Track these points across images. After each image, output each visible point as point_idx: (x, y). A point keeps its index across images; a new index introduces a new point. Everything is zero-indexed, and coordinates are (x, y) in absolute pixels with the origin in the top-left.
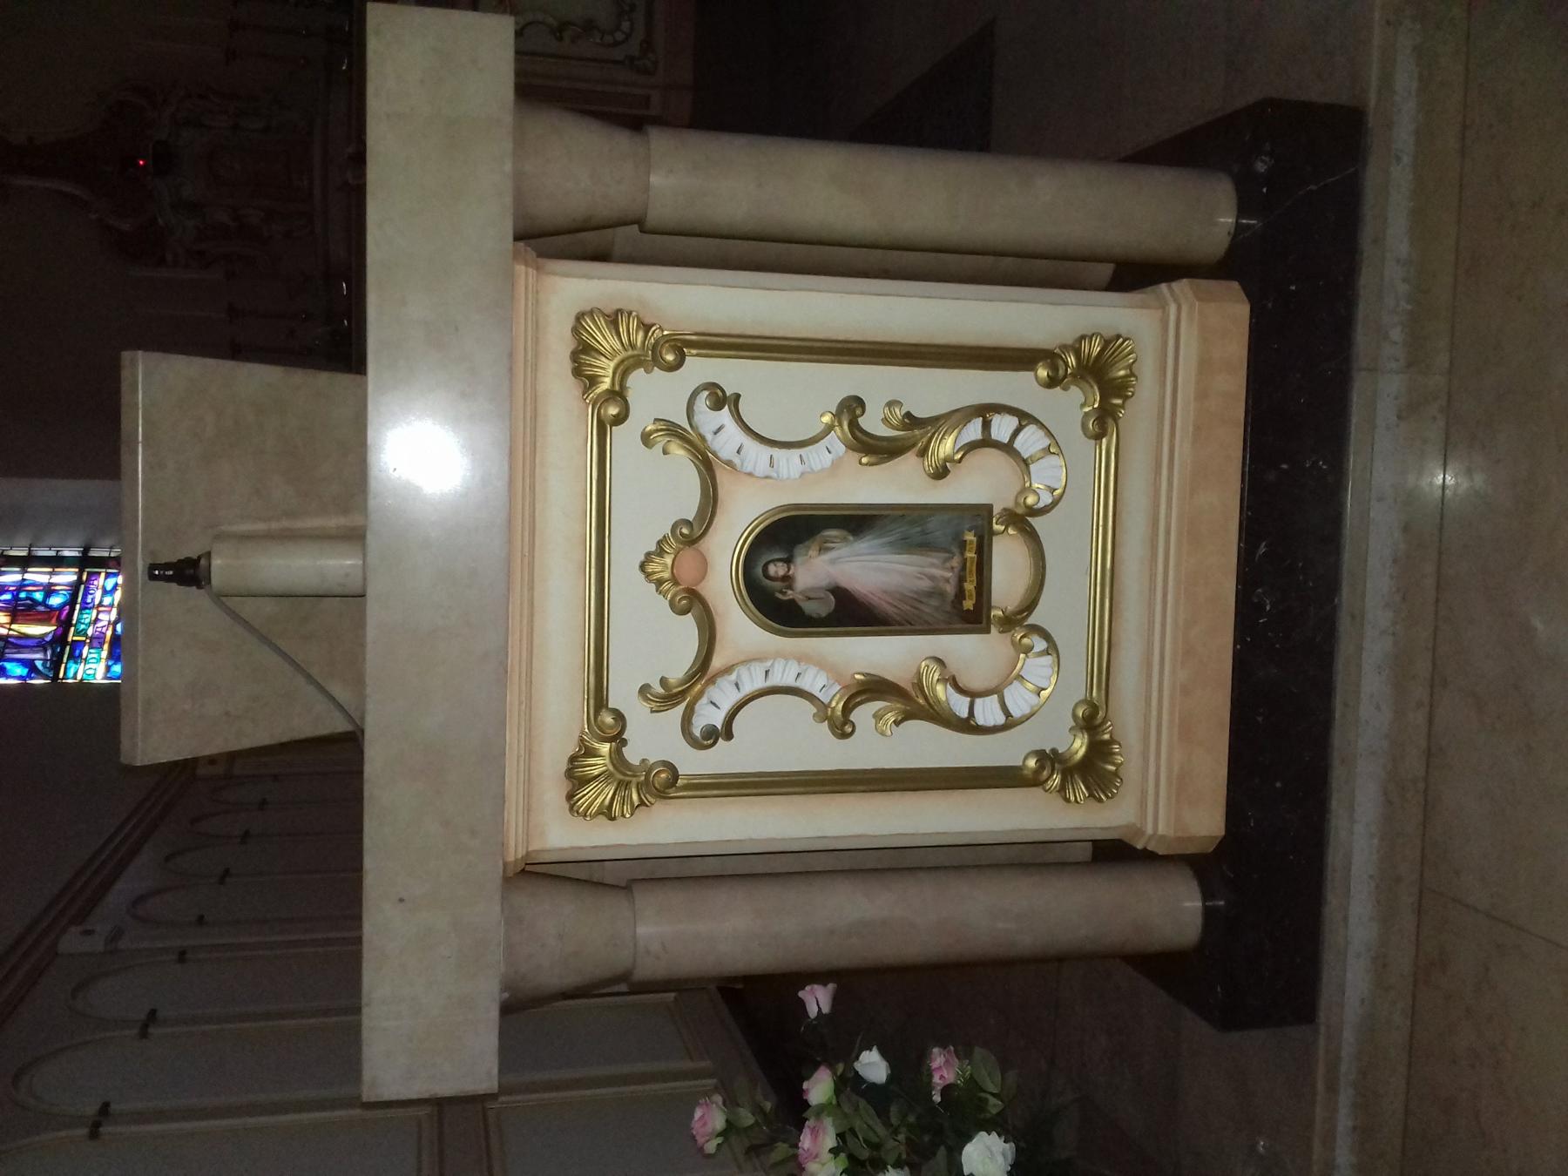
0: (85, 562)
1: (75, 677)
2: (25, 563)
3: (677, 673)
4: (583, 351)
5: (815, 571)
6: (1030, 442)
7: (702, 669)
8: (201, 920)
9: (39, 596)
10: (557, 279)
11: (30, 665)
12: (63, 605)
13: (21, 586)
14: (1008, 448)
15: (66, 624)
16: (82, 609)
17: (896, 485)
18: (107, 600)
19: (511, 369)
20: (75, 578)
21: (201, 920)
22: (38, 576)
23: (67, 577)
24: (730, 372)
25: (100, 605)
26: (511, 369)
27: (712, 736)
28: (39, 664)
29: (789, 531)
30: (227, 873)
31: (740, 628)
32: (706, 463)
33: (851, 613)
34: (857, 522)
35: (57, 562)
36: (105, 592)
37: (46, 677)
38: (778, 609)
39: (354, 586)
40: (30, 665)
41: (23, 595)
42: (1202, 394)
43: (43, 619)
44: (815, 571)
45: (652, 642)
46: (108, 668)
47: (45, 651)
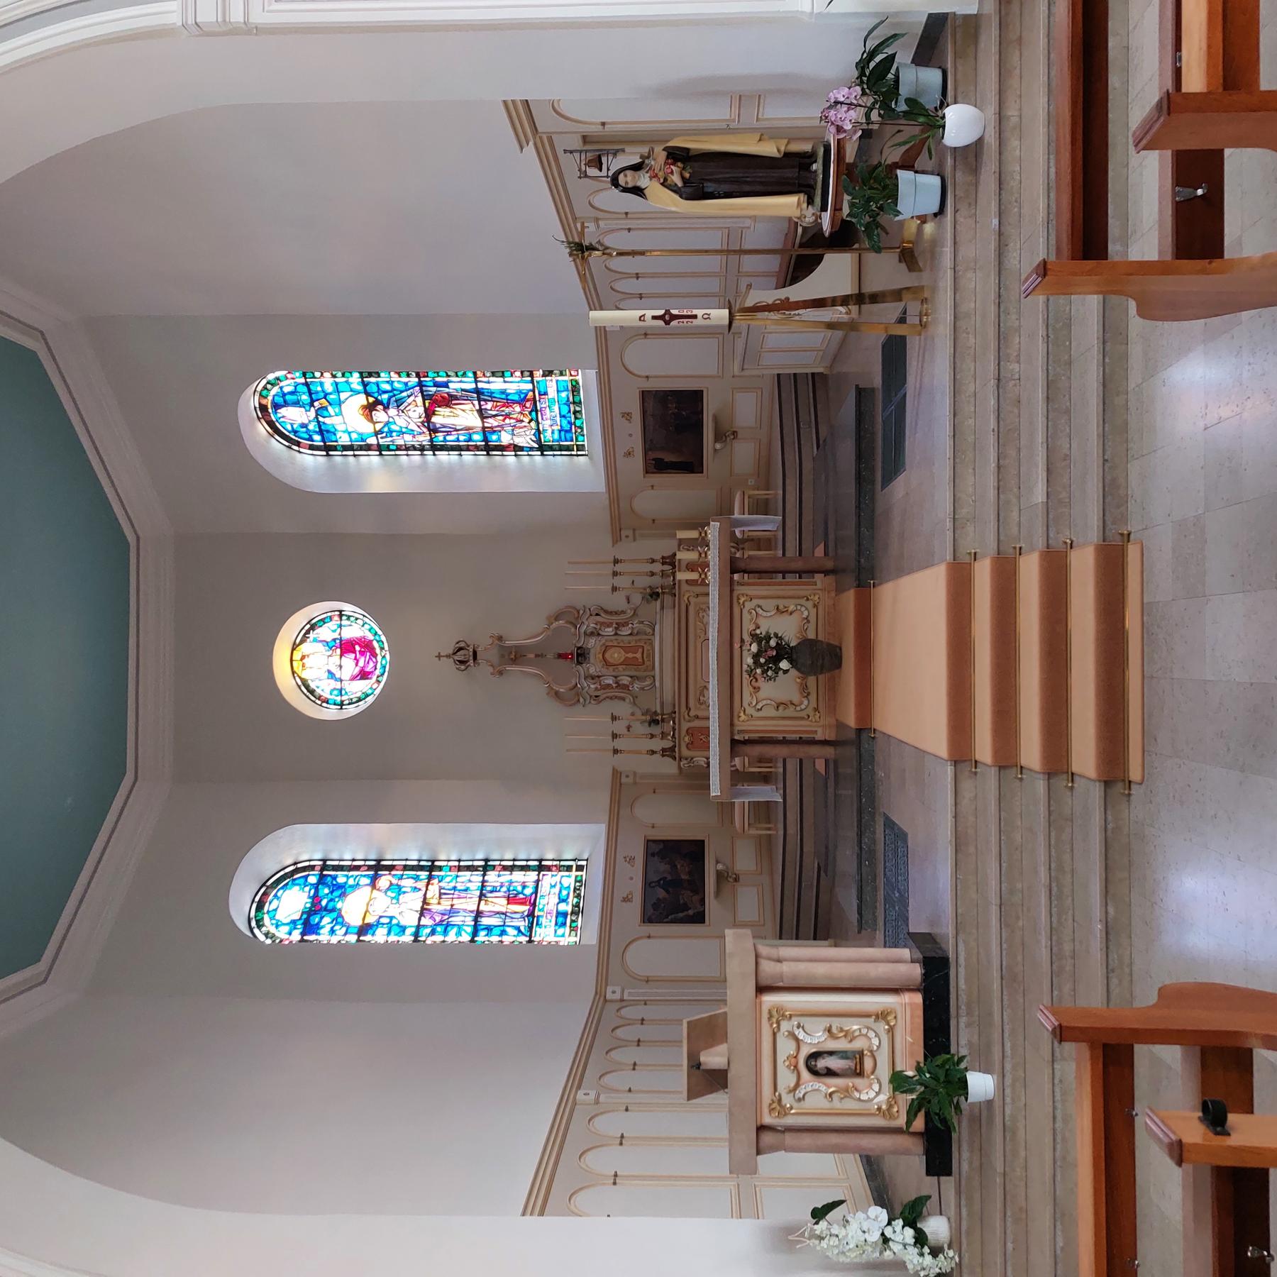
3: (792, 1085)
4: (771, 1016)
5: (821, 1064)
6: (872, 1034)
7: (797, 1085)
8: (630, 1090)
11: (518, 929)
13: (511, 883)
14: (866, 1035)
15: (534, 905)
17: (841, 1045)
21: (630, 1090)
22: (518, 876)
24: (803, 1020)
27: (799, 1100)
28: (522, 929)
29: (815, 1056)
30: (635, 1064)
31: (805, 1074)
32: (797, 1040)
33: (830, 1073)
34: (831, 1053)
38: (814, 1072)
40: (518, 929)
42: (912, 1023)
43: (523, 902)
44: (821, 1064)
45: (786, 1079)
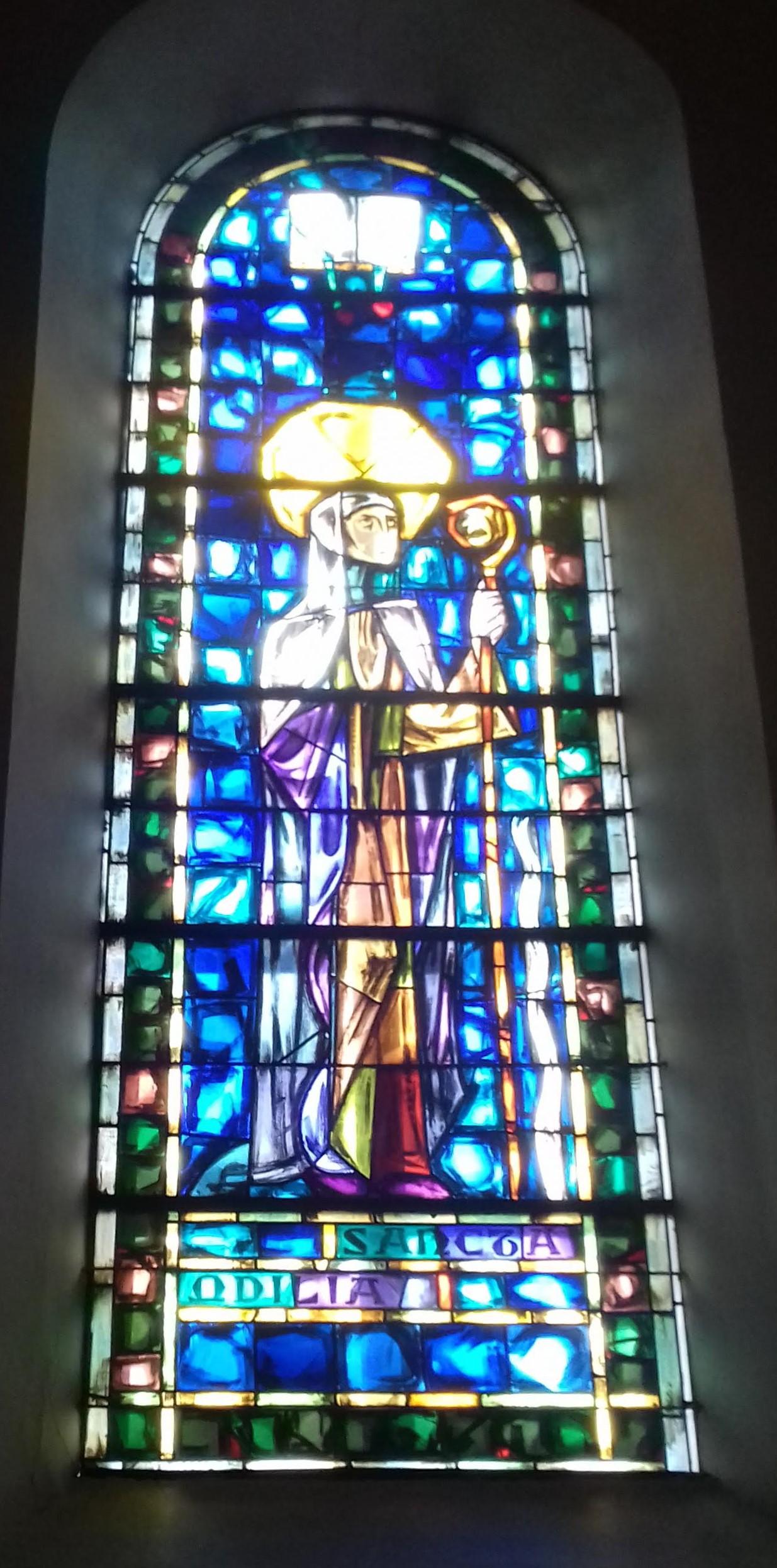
0: (618, 1215)
1: (188, 1251)
2: (605, 1059)
9: (482, 1114)
10: (124, 951)
12: (453, 1183)
14: (334, 263)
16: (439, 1232)
18: (477, 1293)
19: (276, 999)
20: (555, 1192)
22: (560, 1098)
23: (563, 1171)
25: (457, 1276)
26: (276, 999)
35: (614, 1127)
36: (508, 1287)
37: (188, 1180)
39: (607, 640)
41: (482, 1076)
46: (220, 1332)
47: (282, 1163)
